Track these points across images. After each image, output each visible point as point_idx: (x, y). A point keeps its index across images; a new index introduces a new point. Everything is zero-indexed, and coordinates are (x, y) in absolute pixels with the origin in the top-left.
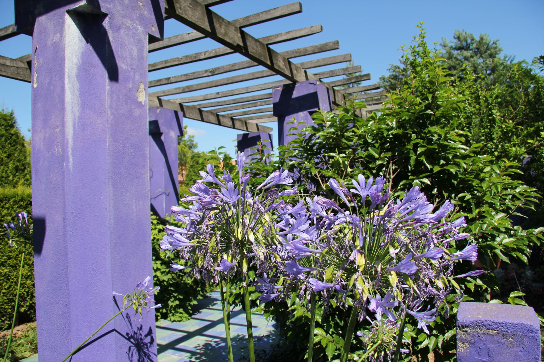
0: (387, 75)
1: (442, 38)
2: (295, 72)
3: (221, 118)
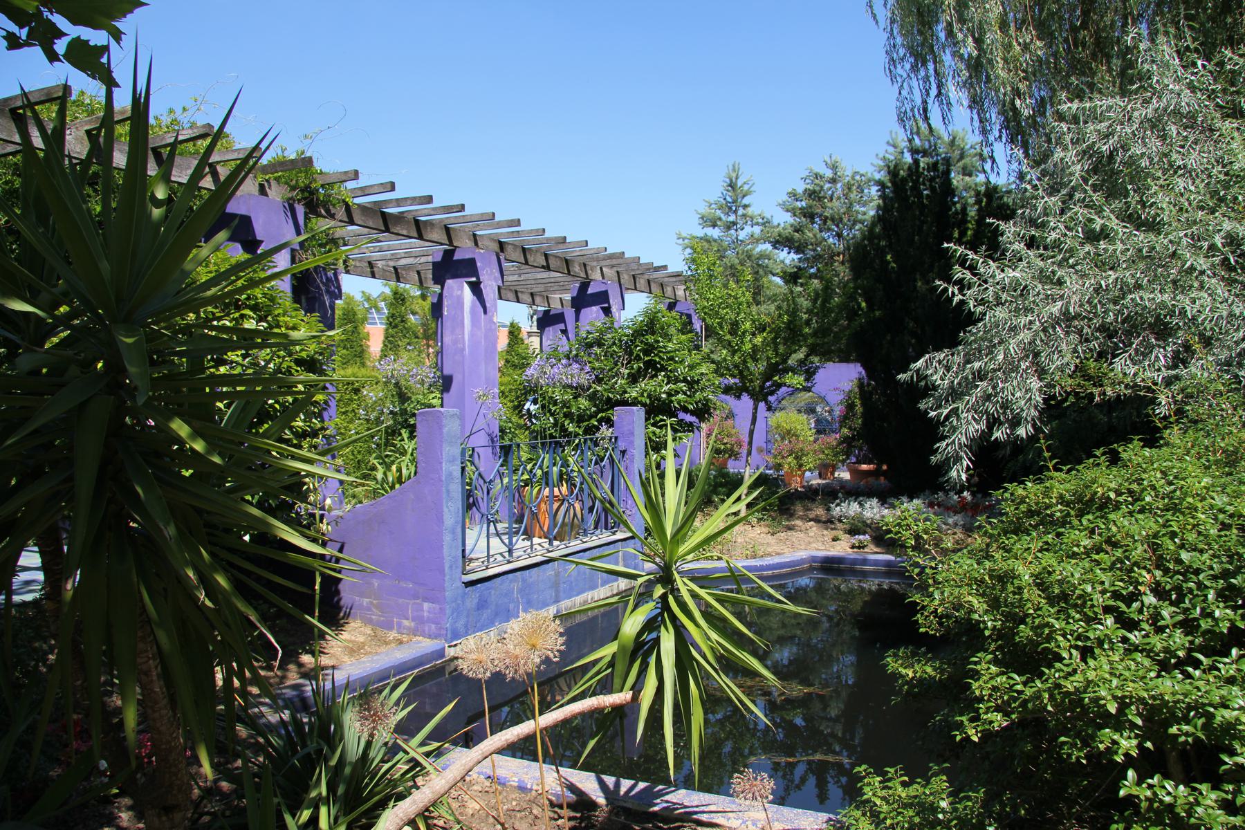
0: (800, 188)
1: (891, 132)
2: (590, 272)
3: (520, 295)
